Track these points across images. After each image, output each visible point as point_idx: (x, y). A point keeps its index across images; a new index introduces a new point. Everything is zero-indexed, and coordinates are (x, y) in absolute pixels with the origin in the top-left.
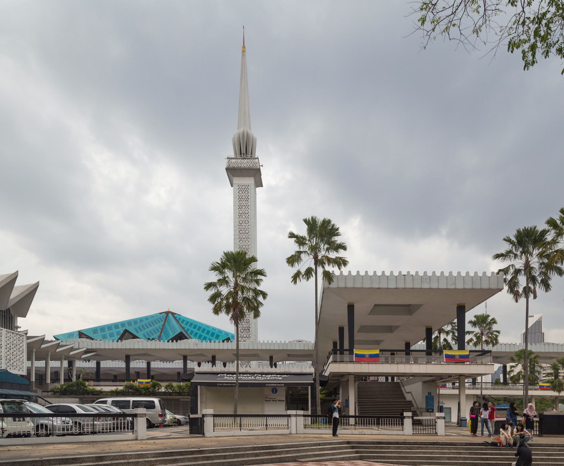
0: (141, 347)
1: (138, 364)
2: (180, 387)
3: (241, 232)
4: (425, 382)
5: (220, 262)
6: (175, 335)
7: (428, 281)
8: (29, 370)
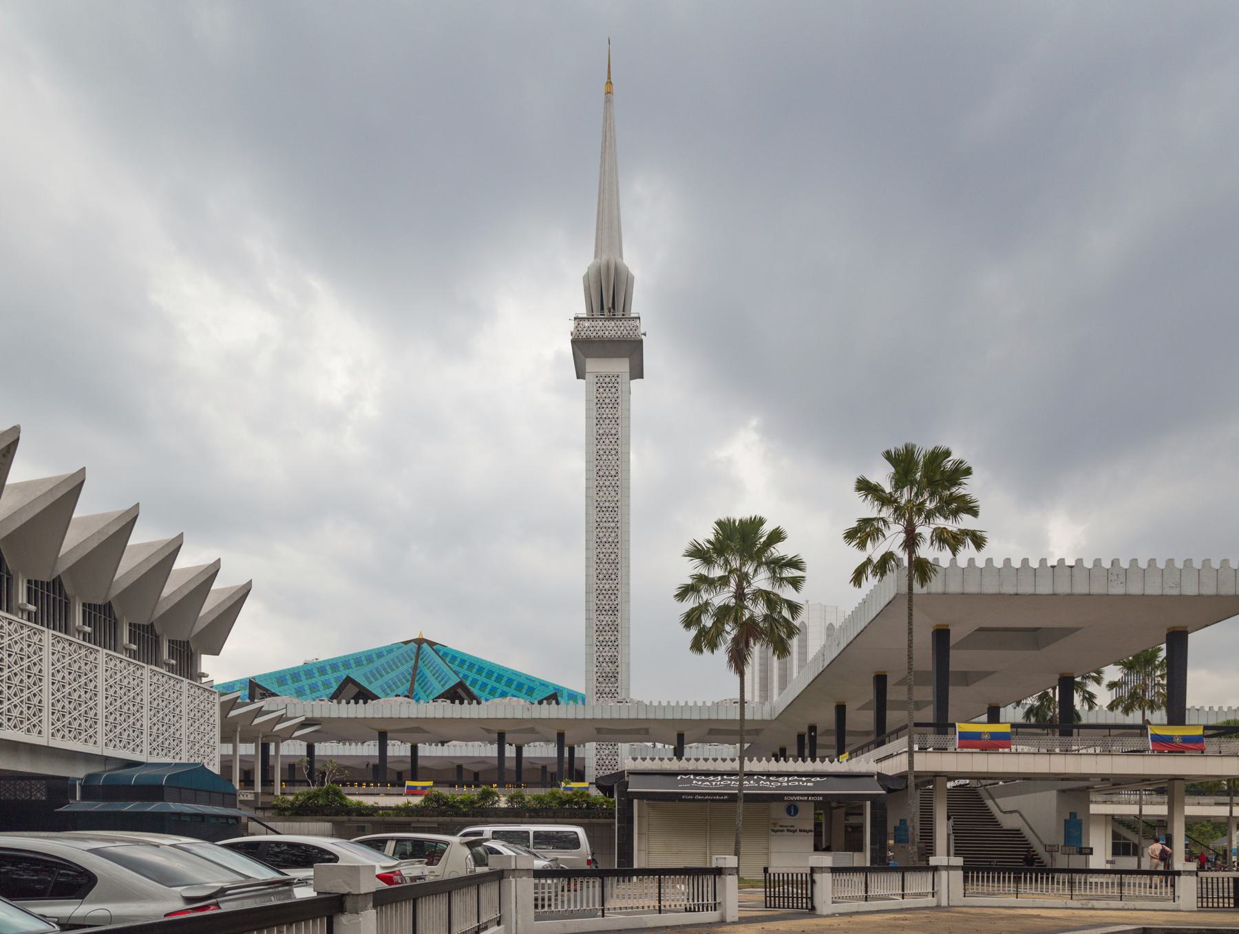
0: (413, 716)
1: (398, 749)
2: (540, 799)
3: (601, 473)
4: (1062, 792)
5: (712, 538)
6: (447, 687)
7: (1122, 579)
8: (226, 765)
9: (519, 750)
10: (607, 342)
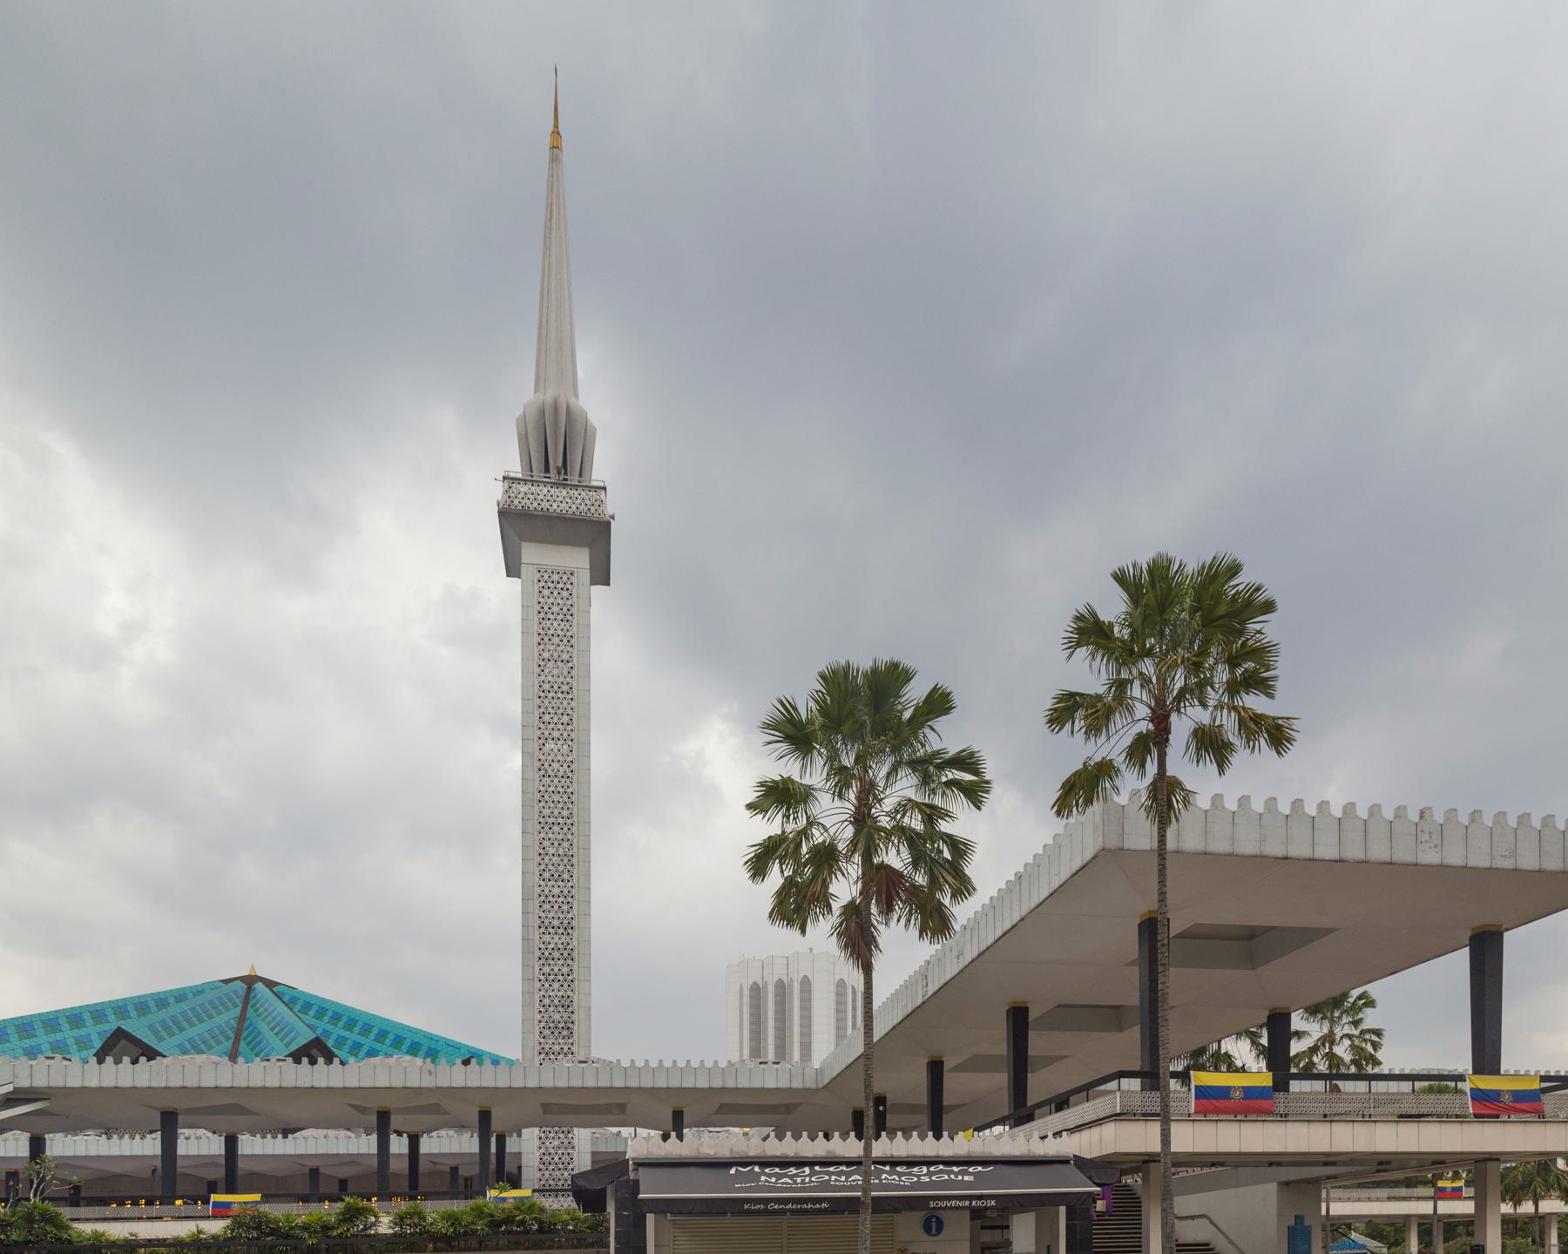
0: (225, 1083)
1: (198, 1144)
2: (453, 1219)
3: (546, 718)
9: (414, 1141)
10: (554, 521)
